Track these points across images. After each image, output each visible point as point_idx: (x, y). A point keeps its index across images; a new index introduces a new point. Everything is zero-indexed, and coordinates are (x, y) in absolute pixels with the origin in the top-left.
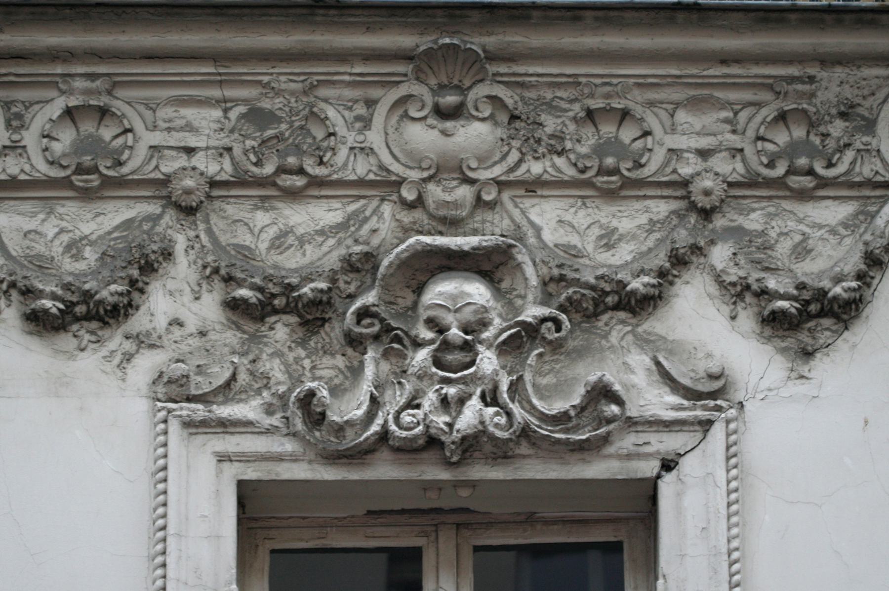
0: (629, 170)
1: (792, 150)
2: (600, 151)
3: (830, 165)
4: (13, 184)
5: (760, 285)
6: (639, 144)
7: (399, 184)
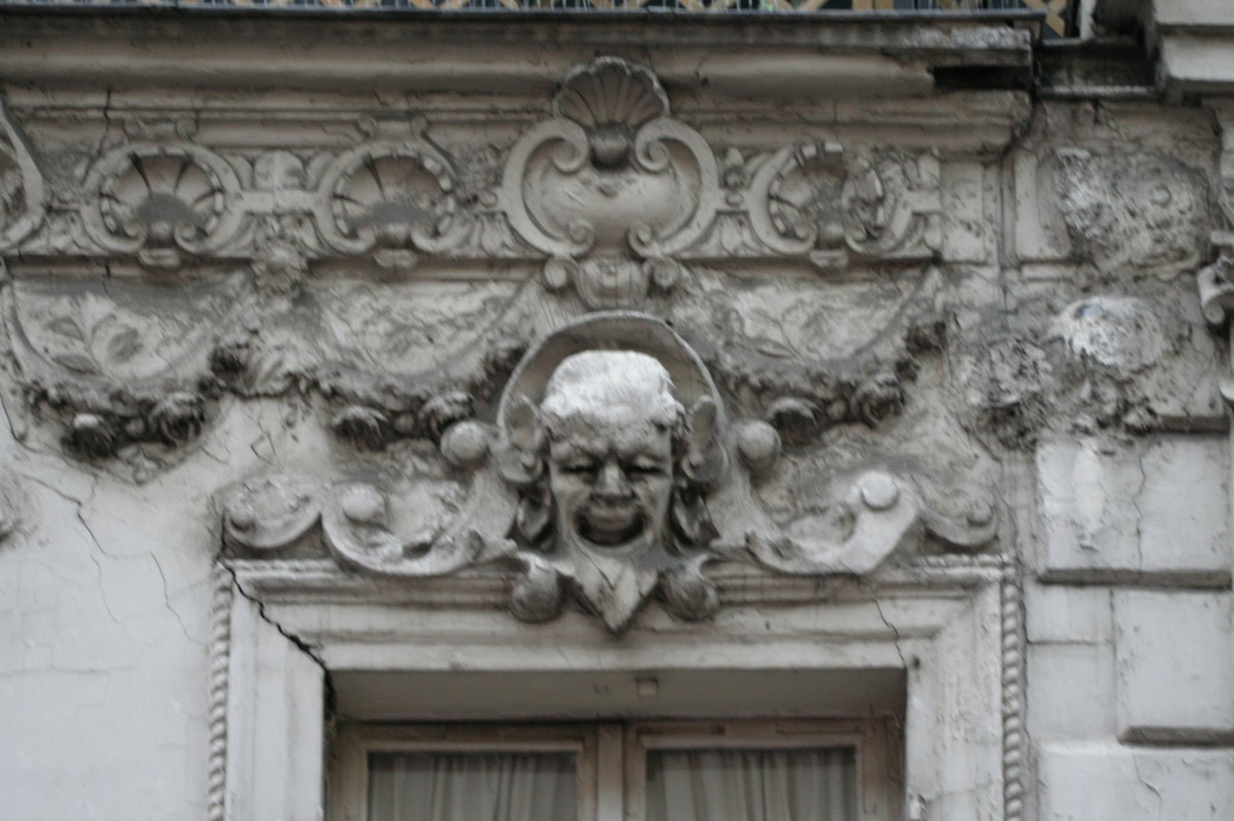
0: (858, 242)
1: (382, 213)
2: (146, 213)
3: (436, 234)
4: (21, 263)
5: (61, 392)
6: (202, 207)
7: (542, 261)
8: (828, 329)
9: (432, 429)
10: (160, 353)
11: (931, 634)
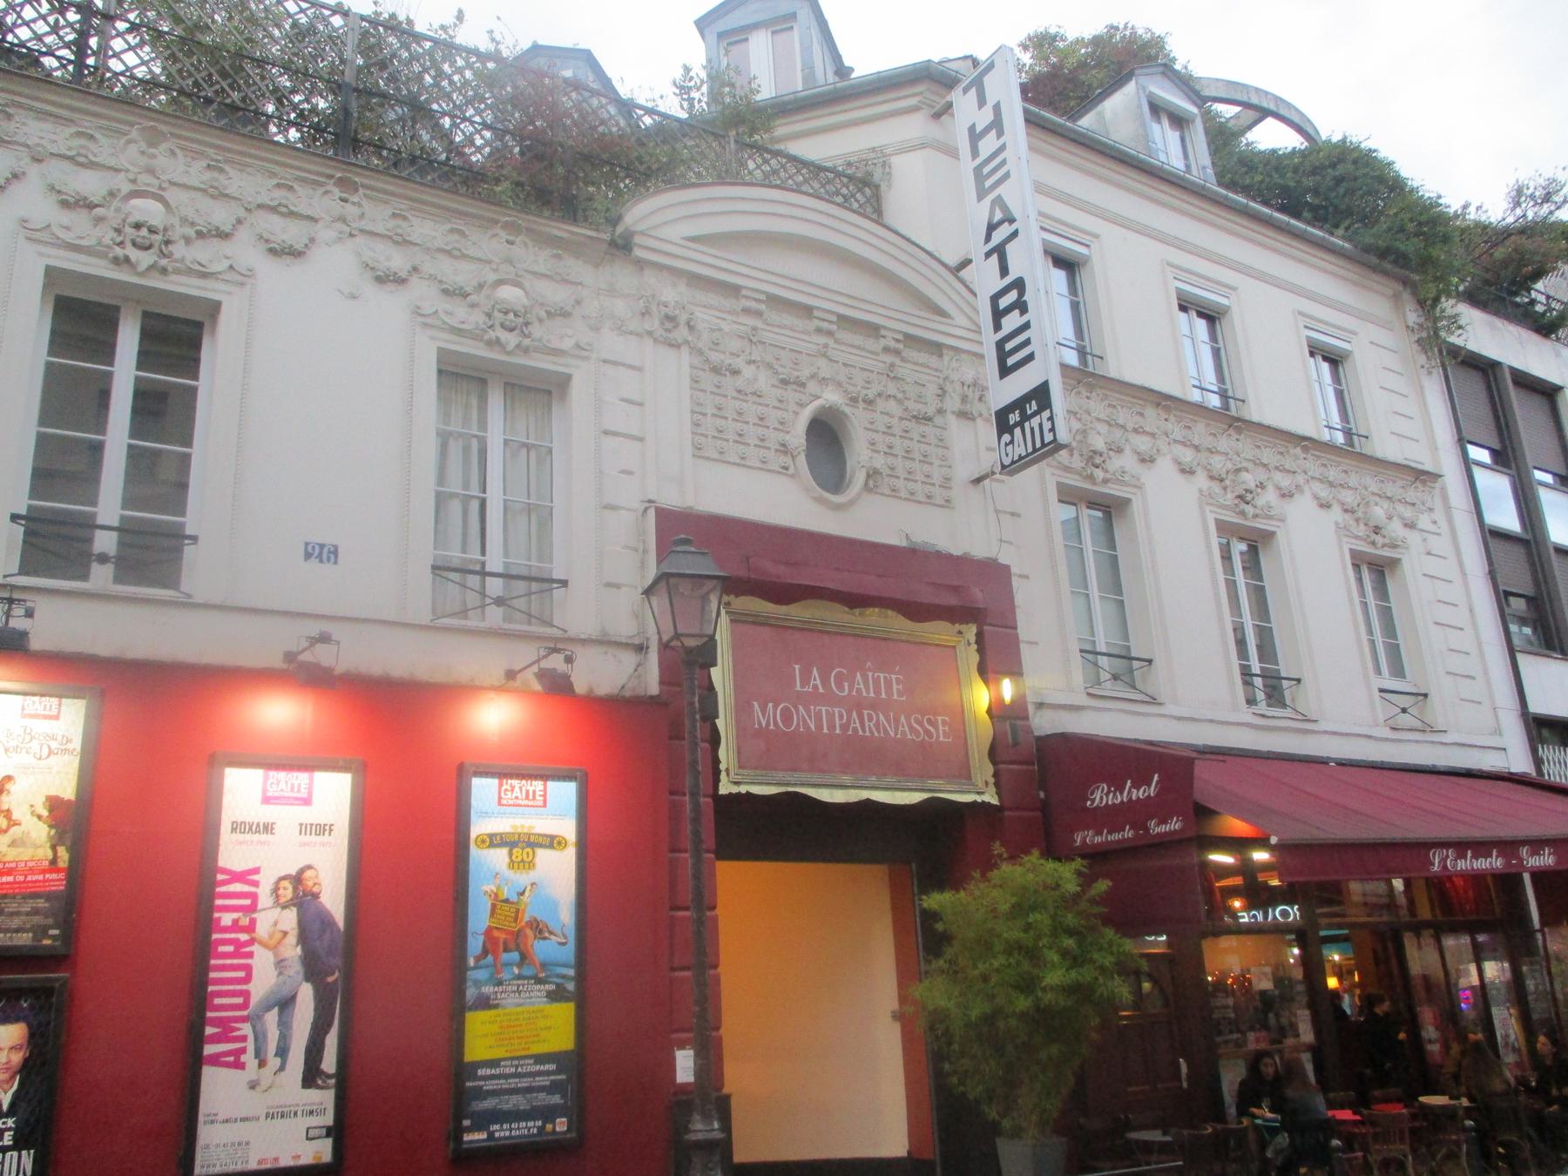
8: (557, 295)
9: (466, 295)
10: (397, 261)
11: (230, 293)
